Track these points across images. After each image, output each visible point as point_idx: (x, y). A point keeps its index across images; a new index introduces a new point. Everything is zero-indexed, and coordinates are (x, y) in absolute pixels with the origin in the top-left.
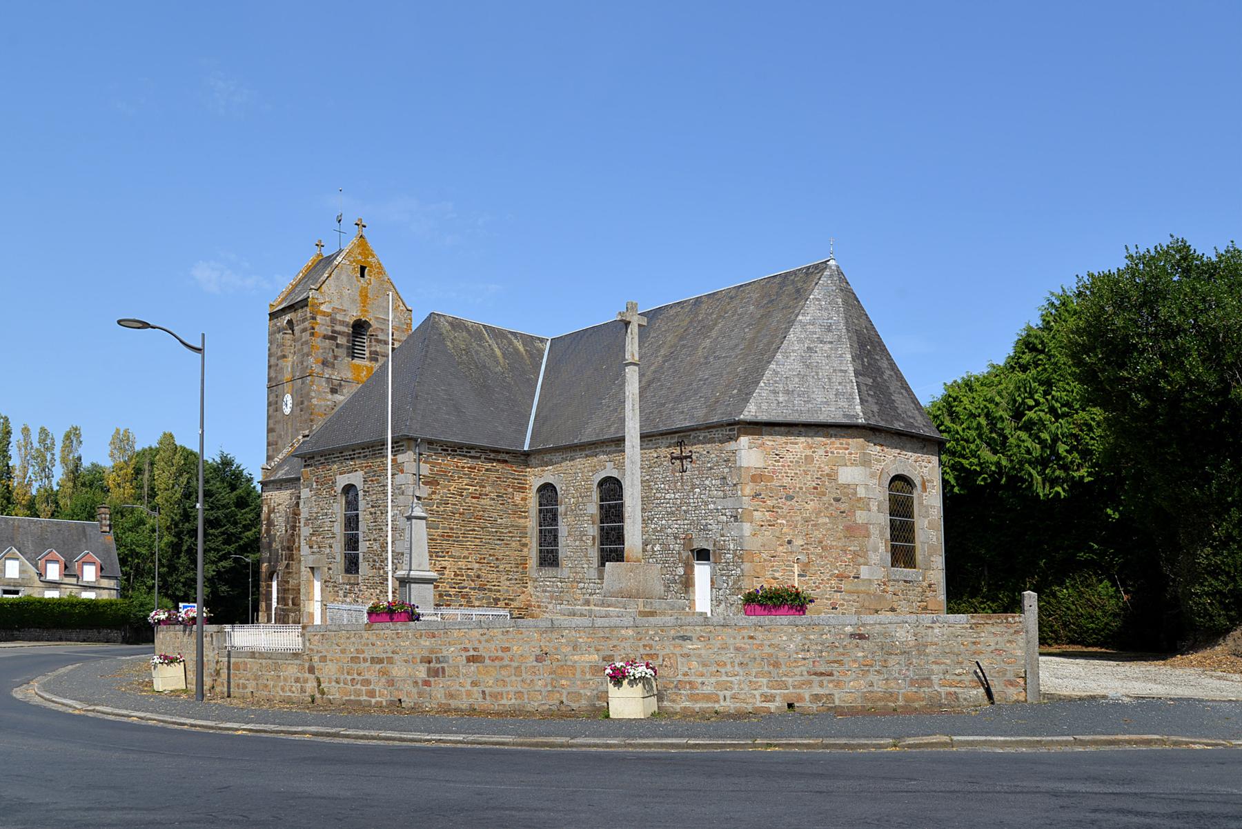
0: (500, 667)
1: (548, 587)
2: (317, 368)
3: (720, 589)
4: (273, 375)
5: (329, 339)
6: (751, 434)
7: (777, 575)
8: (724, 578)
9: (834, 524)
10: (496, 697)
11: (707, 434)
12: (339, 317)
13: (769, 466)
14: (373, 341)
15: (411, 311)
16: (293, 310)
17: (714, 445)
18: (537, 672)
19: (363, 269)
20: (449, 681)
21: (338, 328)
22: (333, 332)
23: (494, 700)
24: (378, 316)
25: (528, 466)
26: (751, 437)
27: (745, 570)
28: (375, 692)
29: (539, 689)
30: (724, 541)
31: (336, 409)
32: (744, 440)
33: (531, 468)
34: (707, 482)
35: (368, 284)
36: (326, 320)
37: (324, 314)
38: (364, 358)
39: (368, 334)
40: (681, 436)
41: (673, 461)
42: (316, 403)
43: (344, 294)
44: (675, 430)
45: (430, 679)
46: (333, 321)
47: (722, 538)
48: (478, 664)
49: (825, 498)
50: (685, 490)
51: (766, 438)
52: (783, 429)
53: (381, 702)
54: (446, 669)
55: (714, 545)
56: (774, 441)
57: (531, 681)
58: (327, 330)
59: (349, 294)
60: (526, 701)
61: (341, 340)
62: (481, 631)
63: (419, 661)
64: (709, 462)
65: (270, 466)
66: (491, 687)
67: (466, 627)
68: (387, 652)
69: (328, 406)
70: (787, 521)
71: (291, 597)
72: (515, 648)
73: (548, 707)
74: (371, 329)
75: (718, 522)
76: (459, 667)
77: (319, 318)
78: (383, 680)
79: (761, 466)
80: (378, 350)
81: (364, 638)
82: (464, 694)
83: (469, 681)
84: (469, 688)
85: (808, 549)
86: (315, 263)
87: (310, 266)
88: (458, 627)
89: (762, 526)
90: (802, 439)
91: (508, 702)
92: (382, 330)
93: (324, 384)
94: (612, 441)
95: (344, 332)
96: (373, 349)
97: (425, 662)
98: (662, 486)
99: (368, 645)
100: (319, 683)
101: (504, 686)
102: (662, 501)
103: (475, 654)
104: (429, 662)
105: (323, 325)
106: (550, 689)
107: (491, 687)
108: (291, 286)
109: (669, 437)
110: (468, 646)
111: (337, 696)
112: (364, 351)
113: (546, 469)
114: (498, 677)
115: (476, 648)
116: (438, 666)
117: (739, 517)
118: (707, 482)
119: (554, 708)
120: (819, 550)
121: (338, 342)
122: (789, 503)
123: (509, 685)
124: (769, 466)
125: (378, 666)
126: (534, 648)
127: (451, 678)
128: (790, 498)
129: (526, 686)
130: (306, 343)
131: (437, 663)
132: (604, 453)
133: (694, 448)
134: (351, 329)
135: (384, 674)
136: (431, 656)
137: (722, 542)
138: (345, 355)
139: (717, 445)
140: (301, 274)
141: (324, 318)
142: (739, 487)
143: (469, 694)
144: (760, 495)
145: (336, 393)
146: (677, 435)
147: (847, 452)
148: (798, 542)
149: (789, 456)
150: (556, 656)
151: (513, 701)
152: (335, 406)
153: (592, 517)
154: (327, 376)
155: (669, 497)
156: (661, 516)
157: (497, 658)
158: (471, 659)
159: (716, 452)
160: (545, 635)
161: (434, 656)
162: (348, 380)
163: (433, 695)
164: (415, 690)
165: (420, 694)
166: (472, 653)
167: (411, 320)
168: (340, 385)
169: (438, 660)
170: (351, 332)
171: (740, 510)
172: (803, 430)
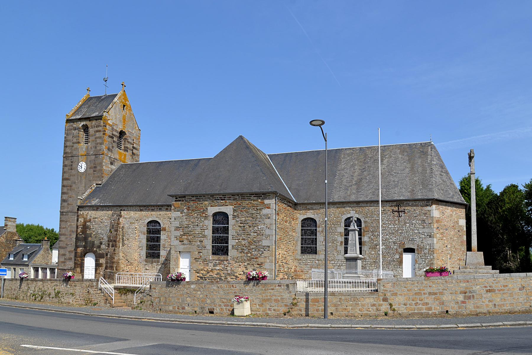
0: (503, 294)
1: (309, 263)
2: (106, 151)
3: (421, 264)
4: (68, 150)
5: (111, 138)
6: (436, 205)
7: (443, 258)
8: (423, 260)
9: (458, 240)
10: (501, 306)
11: (414, 203)
12: (115, 128)
13: (441, 217)
14: (126, 141)
15: (140, 130)
16: (88, 120)
17: (418, 207)
18: (520, 295)
19: (124, 106)
20: (476, 301)
21: (114, 133)
22: (113, 134)
23: (500, 307)
24: (129, 130)
25: (295, 209)
26: (436, 205)
27: (435, 256)
28: (432, 308)
29: (521, 301)
30: (423, 245)
31: (112, 172)
32: (434, 206)
33: (297, 210)
34: (414, 222)
35: (126, 114)
36: (110, 128)
37: (109, 125)
38: (121, 149)
39: (123, 138)
40: (399, 203)
41: (393, 212)
42: (105, 168)
43: (117, 117)
44: (417, 199)
45: (466, 300)
46: (113, 129)
47: (422, 244)
48: (492, 293)
49: (456, 230)
50: (400, 224)
51: (440, 206)
52: (444, 203)
53: (435, 313)
54: (475, 296)
55: (418, 246)
56: (442, 208)
57: (518, 298)
58: (110, 133)
59: (119, 117)
60: (515, 307)
61: (115, 139)
62: (493, 279)
63: (459, 293)
64: (414, 214)
65: (82, 198)
66: (498, 302)
67: (486, 277)
68: (439, 290)
69: (109, 170)
70: (446, 238)
71: (115, 266)
72: (510, 285)
73: (524, 308)
74: (125, 136)
75: (420, 237)
76: (482, 294)
77: (107, 126)
78: (437, 302)
79: (438, 217)
80: (128, 146)
81: (424, 284)
82: (485, 306)
83: (488, 300)
84: (488, 303)
85: (451, 249)
86: (87, 99)
87: (85, 99)
88: (481, 278)
89: (439, 240)
90: (449, 208)
91: (507, 308)
92: (130, 137)
93: (108, 159)
94: (355, 202)
95: (116, 135)
96: (126, 145)
97: (463, 293)
98: (387, 222)
99: (426, 287)
100: (391, 305)
101: (505, 301)
102: (386, 228)
103: (490, 288)
104: (465, 293)
105: (109, 130)
106: (526, 301)
107: (498, 302)
108: (76, 108)
109: (391, 203)
110: (487, 285)
111: (405, 311)
112: (121, 146)
113: (309, 211)
114: (502, 298)
115: (491, 286)
116: (470, 294)
117: (432, 236)
118: (414, 222)
119: (528, 309)
120: (454, 250)
121: (114, 140)
122: (446, 231)
123: (507, 301)
124: (441, 217)
125: (433, 296)
126: (519, 285)
127: (478, 300)
128: (447, 230)
129: (515, 301)
130: (100, 138)
131: (470, 293)
132: (349, 207)
133: (406, 208)
134: (119, 135)
135: (437, 299)
136: (466, 290)
137: (422, 246)
138: (116, 147)
139: (420, 208)
140: (81, 103)
141: (109, 127)
142: (432, 224)
143: (487, 306)
144: (439, 228)
145: (113, 165)
146: (395, 202)
147: (461, 214)
148: (449, 246)
149: (446, 214)
150: (528, 288)
151: (509, 307)
152: (112, 171)
153: (340, 233)
154: (109, 156)
155: (391, 227)
156: (386, 234)
157: (501, 290)
158: (488, 290)
159: (419, 210)
160: (523, 280)
161: (468, 290)
162: (117, 159)
163: (467, 307)
164: (456, 306)
165: (459, 308)
166: (489, 288)
167: (140, 134)
168: (114, 161)
169: (470, 292)
170: (119, 136)
171: (432, 233)
172: (450, 204)
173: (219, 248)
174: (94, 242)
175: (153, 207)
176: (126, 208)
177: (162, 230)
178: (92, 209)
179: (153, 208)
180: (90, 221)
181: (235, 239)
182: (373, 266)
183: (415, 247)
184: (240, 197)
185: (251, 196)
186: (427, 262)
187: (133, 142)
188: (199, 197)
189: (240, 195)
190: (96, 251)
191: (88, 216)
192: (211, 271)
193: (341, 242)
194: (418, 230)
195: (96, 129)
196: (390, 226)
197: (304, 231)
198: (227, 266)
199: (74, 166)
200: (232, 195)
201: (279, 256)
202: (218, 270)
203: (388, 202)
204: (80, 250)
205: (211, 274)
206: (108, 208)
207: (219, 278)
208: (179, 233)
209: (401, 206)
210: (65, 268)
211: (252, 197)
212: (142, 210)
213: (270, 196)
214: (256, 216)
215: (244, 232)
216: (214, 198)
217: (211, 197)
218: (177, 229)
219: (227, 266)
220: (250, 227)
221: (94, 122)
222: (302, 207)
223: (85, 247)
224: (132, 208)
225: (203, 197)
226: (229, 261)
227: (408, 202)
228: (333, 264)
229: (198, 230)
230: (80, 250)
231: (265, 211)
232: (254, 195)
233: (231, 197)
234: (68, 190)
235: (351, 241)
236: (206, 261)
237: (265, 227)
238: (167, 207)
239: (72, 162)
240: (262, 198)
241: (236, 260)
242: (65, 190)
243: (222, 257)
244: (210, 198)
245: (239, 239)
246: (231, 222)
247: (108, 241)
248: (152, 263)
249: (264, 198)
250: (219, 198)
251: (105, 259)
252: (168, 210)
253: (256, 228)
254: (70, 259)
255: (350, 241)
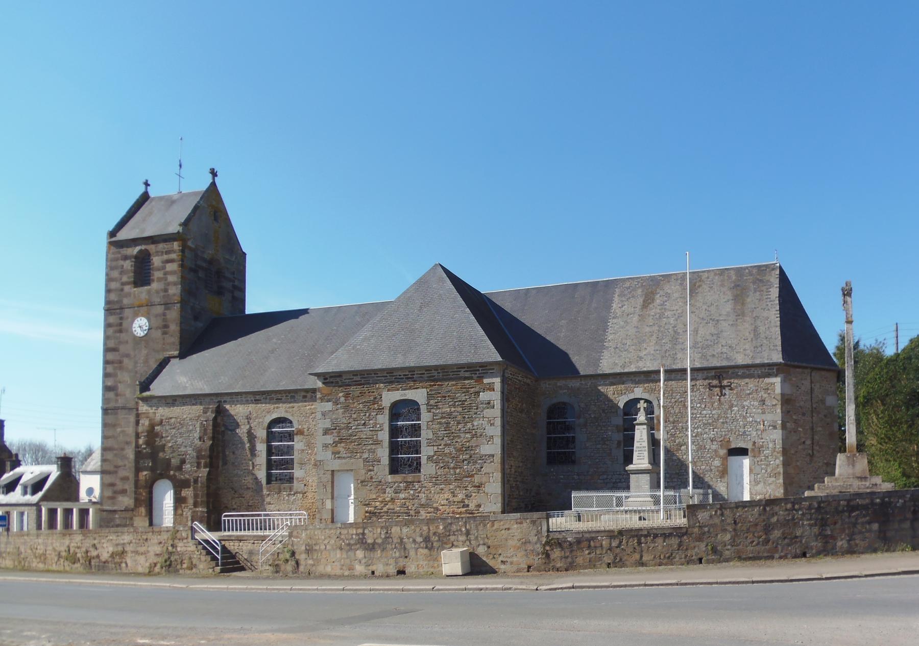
3: (759, 474)
21: (199, 263)
30: (763, 442)
98: (698, 405)
109: (705, 372)
146: (714, 371)
173: (404, 463)
174: (169, 460)
175: (280, 394)
176: (229, 397)
177: (297, 434)
178: (164, 402)
179: (279, 396)
180: (161, 423)
181: (433, 446)
182: (676, 480)
183: (749, 446)
184: (439, 373)
185: (460, 371)
186: (769, 470)
187: (234, 277)
188: (366, 376)
189: (441, 370)
190: (174, 475)
191: (157, 415)
192: (389, 501)
193: (619, 442)
194: (753, 417)
195: (165, 257)
196: (705, 412)
197: (551, 425)
198: (419, 492)
199: (125, 325)
200: (426, 371)
201: (511, 471)
202: (403, 499)
203: (701, 372)
204: (144, 474)
205: (390, 506)
206: (195, 399)
207: (406, 513)
208: (329, 439)
209: (724, 376)
210: (115, 508)
211: (462, 372)
212: (258, 400)
213: (493, 369)
214: (470, 404)
215: (449, 433)
216: (393, 376)
217: (388, 375)
218: (326, 432)
219: (419, 492)
220: (459, 423)
221: (161, 246)
222: (549, 384)
223: (152, 469)
224: (239, 397)
225: (373, 375)
226: (422, 483)
227: (737, 370)
228: (603, 479)
229: (366, 432)
230: (144, 474)
231: (484, 396)
232: (465, 368)
233: (424, 374)
234: (115, 369)
235: (639, 443)
236: (381, 486)
237: (486, 422)
238: (305, 394)
239: (121, 318)
240: (479, 374)
241: (435, 480)
242: (110, 369)
243: (410, 477)
244: (387, 376)
245: (440, 445)
246: (425, 416)
247: (198, 457)
248: (279, 492)
249: (484, 373)
250: (402, 377)
251: (191, 489)
252: (307, 399)
253: (469, 425)
254: (124, 492)
255: (637, 442)
